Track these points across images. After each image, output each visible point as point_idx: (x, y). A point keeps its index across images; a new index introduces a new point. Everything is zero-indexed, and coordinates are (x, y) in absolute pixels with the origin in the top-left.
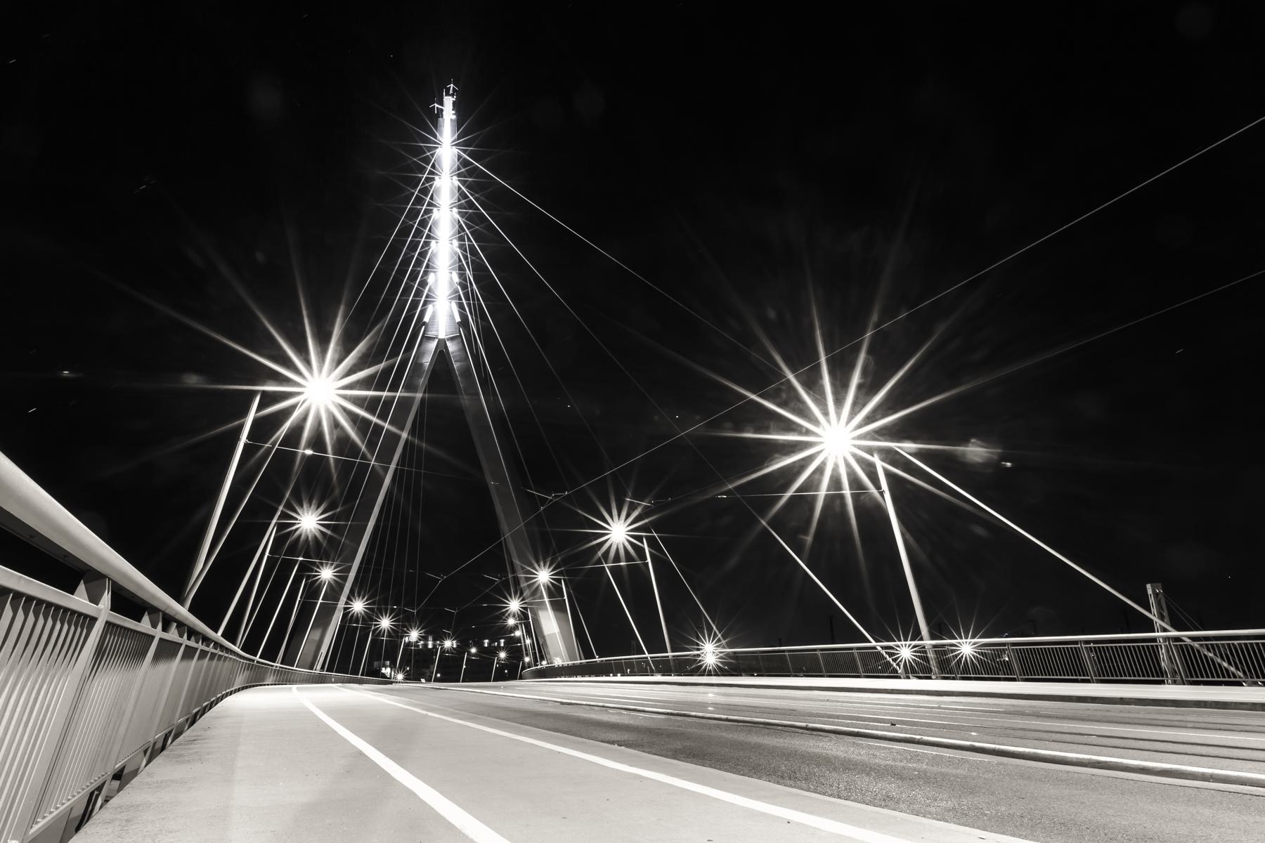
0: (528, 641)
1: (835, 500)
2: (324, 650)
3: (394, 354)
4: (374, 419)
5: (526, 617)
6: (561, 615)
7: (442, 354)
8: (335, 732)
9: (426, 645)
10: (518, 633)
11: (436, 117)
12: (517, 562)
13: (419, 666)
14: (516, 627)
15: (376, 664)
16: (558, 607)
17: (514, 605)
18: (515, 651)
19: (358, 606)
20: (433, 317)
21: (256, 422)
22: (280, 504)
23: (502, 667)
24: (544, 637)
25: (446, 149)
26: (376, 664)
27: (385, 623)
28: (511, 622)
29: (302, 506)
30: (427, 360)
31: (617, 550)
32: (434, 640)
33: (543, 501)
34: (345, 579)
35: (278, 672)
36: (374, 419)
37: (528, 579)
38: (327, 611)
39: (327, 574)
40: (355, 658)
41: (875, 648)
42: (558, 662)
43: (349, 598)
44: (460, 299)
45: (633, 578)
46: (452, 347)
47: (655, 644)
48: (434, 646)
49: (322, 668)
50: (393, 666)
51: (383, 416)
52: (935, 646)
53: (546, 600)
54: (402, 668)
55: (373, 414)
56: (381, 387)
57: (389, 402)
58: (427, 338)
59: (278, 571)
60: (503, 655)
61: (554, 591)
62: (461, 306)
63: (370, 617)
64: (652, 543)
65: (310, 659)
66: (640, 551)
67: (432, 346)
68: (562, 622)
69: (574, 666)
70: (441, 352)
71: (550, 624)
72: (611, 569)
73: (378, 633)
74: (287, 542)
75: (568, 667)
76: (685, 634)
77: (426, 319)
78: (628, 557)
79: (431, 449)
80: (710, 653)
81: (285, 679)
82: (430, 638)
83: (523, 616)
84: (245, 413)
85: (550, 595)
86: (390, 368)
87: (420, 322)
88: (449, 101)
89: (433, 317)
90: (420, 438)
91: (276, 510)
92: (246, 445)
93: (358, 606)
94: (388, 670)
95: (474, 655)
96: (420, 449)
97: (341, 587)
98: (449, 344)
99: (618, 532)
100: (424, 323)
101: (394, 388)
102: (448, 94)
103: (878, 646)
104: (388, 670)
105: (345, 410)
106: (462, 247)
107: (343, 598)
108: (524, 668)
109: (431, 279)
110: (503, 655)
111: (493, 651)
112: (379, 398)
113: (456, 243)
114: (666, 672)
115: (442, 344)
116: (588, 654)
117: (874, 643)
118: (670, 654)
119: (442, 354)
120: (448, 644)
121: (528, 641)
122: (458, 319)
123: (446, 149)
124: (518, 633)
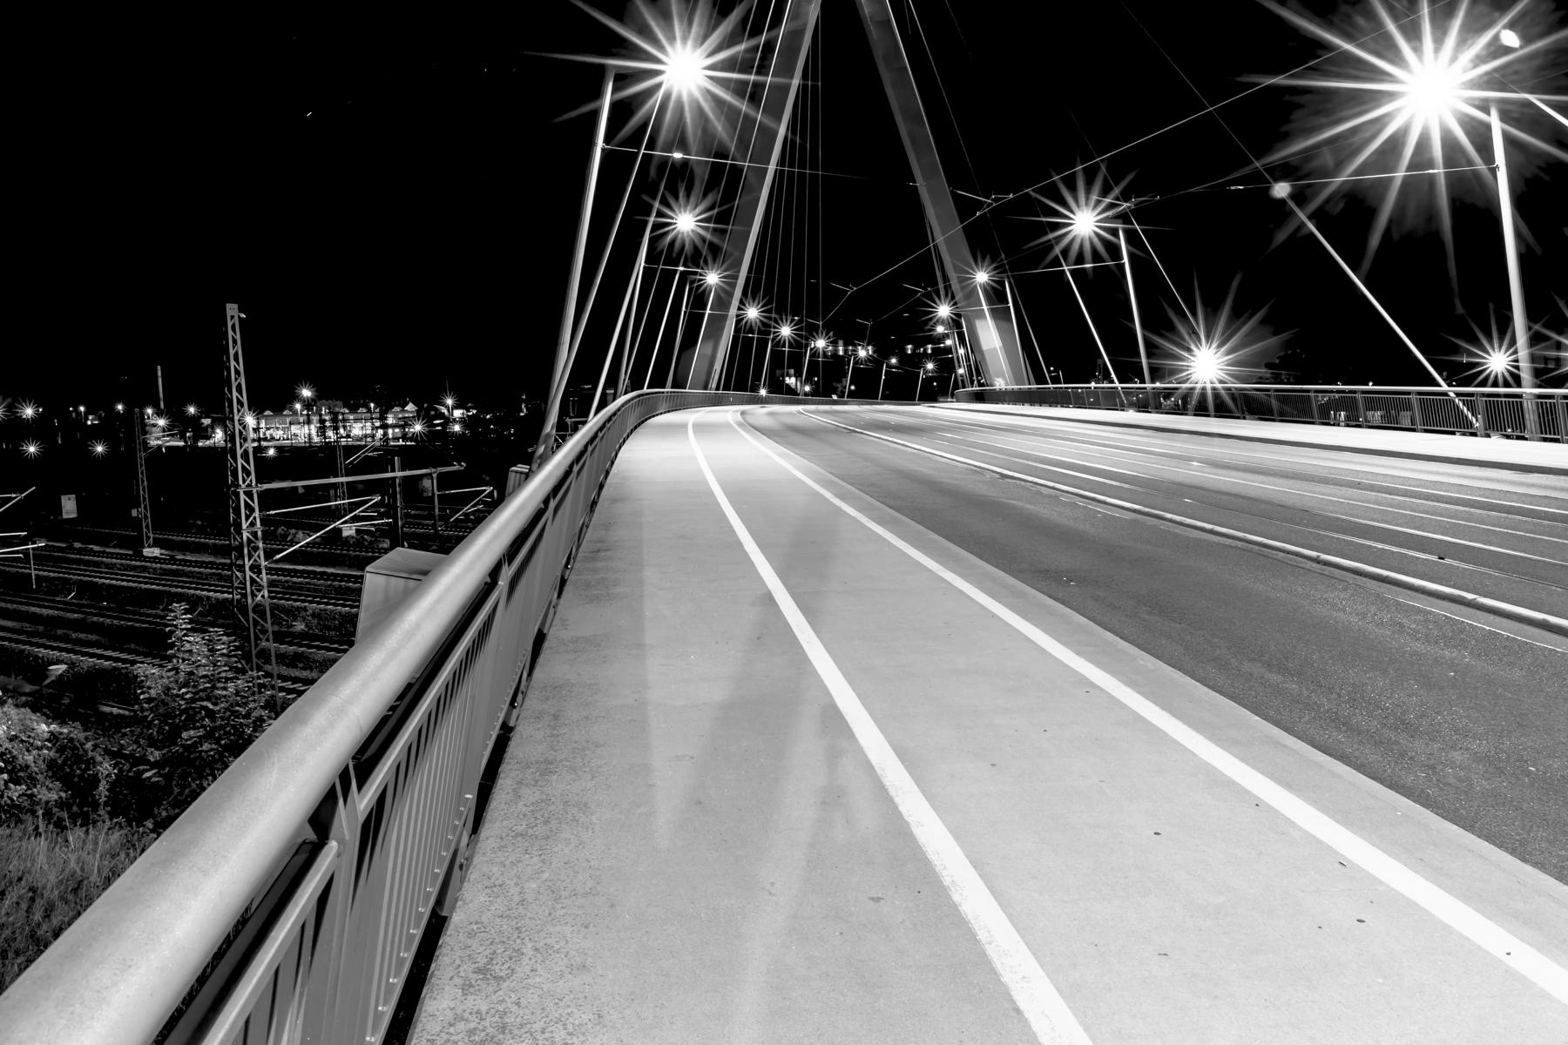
0: (961, 351)
2: (717, 367)
3: (776, 22)
5: (959, 326)
6: (1004, 324)
8: (739, 544)
10: (949, 342)
13: (828, 381)
14: (946, 336)
15: (778, 372)
16: (1000, 315)
17: (944, 310)
18: (946, 362)
21: (613, 105)
22: (649, 215)
23: (928, 381)
24: (981, 352)
26: (778, 372)
27: (786, 331)
31: (1081, 246)
32: (846, 345)
33: (980, 205)
34: (733, 286)
35: (671, 397)
38: (718, 322)
39: (712, 278)
40: (753, 371)
41: (1445, 394)
42: (1000, 384)
43: (741, 302)
45: (1102, 283)
47: (1129, 371)
48: (846, 351)
50: (798, 375)
52: (1540, 396)
53: (985, 307)
54: (808, 380)
59: (657, 284)
61: (995, 294)
63: (765, 328)
64: (1132, 237)
65: (703, 378)
66: (1114, 250)
68: (1004, 334)
69: (1020, 392)
71: (990, 336)
72: (1073, 272)
73: (778, 343)
74: (667, 254)
75: (1013, 392)
78: (1096, 257)
80: (1207, 364)
81: (679, 405)
82: (841, 342)
83: (955, 322)
84: (598, 94)
85: (990, 301)
91: (646, 223)
92: (603, 150)
93: (753, 313)
94: (793, 380)
97: (731, 295)
99: (1084, 222)
103: (1451, 391)
104: (793, 380)
105: (711, 78)
107: (733, 311)
108: (956, 387)
110: (930, 366)
111: (918, 360)
114: (1143, 407)
116: (1040, 379)
117: (1445, 387)
118: (1148, 385)
120: (862, 353)
121: (961, 351)
124: (949, 342)
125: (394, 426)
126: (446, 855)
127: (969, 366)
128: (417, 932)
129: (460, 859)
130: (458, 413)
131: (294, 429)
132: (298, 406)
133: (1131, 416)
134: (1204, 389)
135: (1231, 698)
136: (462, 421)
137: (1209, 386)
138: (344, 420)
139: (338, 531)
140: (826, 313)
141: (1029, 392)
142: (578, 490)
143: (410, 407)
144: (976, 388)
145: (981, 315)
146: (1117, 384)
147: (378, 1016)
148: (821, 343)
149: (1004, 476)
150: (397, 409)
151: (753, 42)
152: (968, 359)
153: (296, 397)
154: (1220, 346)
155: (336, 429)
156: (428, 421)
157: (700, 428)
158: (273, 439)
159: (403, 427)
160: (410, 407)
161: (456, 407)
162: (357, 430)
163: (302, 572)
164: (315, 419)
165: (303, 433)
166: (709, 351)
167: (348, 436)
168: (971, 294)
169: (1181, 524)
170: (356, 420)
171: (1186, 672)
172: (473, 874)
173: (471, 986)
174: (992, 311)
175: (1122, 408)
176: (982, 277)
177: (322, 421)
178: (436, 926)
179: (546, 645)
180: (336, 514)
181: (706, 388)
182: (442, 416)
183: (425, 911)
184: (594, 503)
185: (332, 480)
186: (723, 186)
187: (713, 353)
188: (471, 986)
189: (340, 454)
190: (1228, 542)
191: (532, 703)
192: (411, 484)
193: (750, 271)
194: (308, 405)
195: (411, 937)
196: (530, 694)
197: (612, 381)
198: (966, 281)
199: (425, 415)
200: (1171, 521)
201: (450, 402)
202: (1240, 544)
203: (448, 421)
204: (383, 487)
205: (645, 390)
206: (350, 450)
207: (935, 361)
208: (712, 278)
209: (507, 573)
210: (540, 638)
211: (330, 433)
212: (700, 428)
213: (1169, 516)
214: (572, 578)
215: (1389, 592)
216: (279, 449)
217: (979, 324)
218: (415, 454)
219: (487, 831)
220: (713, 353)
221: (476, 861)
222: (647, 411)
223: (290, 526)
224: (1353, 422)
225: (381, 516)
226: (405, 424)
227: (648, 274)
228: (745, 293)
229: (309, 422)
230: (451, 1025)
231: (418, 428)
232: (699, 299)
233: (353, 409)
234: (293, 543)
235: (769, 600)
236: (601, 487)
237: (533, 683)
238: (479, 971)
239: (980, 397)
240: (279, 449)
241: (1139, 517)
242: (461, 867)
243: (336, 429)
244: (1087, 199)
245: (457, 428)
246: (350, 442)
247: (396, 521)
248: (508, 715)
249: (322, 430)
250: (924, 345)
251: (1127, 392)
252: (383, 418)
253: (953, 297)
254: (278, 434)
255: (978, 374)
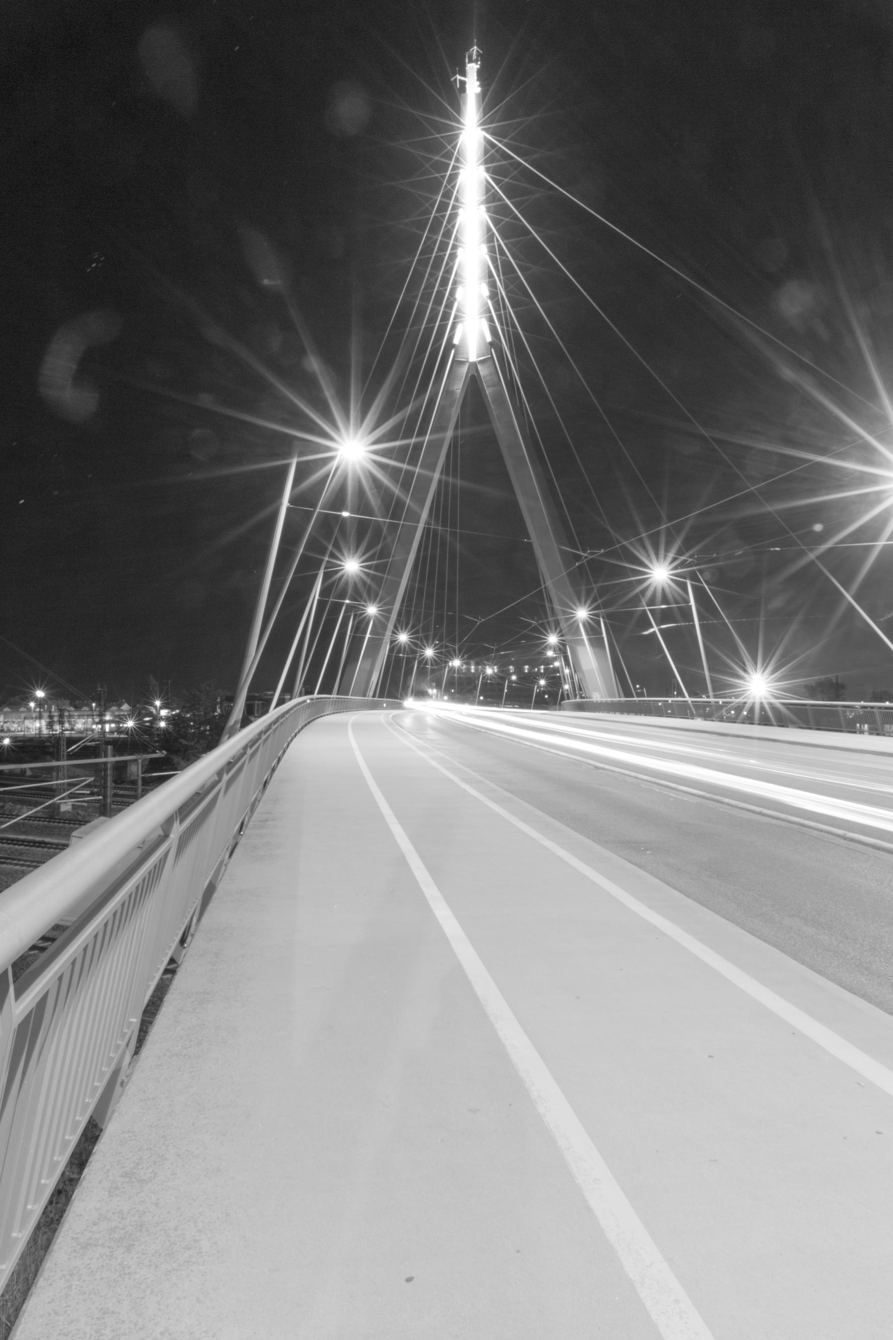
0: (567, 671)
1: (839, 479)
4: (405, 466)
7: (474, 382)
8: (381, 817)
9: (468, 669)
10: (557, 664)
11: (455, 95)
12: (557, 607)
14: (554, 659)
16: (596, 642)
17: (553, 639)
18: (555, 680)
19: (403, 638)
20: (463, 340)
23: (540, 695)
25: (472, 134)
27: (429, 652)
28: (550, 654)
29: (343, 555)
30: (459, 387)
34: (388, 619)
35: (336, 702)
36: (405, 466)
37: (567, 620)
38: (375, 645)
39: (372, 610)
42: (597, 697)
44: (490, 312)
45: (673, 612)
46: (483, 371)
47: (696, 686)
48: (476, 670)
49: (374, 696)
51: (413, 461)
53: (585, 637)
55: (403, 462)
56: (408, 434)
57: (417, 447)
58: (457, 363)
59: (328, 613)
60: (542, 682)
61: (592, 629)
62: (491, 320)
67: (464, 369)
68: (600, 657)
70: (473, 377)
74: (334, 588)
76: (726, 667)
77: (456, 341)
79: (466, 484)
80: (759, 685)
81: (342, 707)
83: (561, 649)
86: (416, 413)
87: (450, 345)
88: (472, 68)
89: (463, 340)
90: (455, 476)
95: (515, 682)
96: (454, 486)
98: (479, 367)
99: (660, 574)
100: (454, 346)
101: (422, 432)
102: (471, 61)
106: (492, 250)
107: (388, 633)
108: (563, 699)
109: (459, 294)
112: (408, 446)
113: (484, 249)
114: (707, 717)
115: (474, 366)
116: (627, 693)
119: (474, 382)
120: (489, 671)
122: (489, 339)
123: (472, 134)
124: (557, 664)
125: (110, 722)
126: (108, 1071)
127: (573, 683)
128: (73, 1139)
129: (122, 1077)
130: (164, 713)
131: (28, 723)
132: (32, 705)
133: (698, 723)
134: (754, 703)
135: (775, 946)
136: (167, 719)
137: (764, 701)
138: (70, 716)
139: (55, 807)
140: (460, 640)
141: (620, 703)
142: (250, 773)
143: (126, 707)
144: (578, 700)
145: (581, 642)
146: (688, 699)
147: (26, 1214)
148: (456, 663)
149: (597, 768)
150: (114, 708)
151: (420, 439)
152: (572, 678)
153: (29, 697)
154: (773, 672)
155: (61, 723)
156: (139, 716)
157: (357, 726)
158: (9, 731)
159: (118, 723)
160: (126, 707)
161: (163, 707)
162: (80, 725)
163: (23, 841)
164: (46, 715)
165: (36, 727)
166: (367, 666)
167: (72, 729)
168: (574, 628)
169: (736, 807)
170: (80, 716)
171: (738, 924)
172: (131, 1089)
173: (117, 1188)
174: (590, 640)
175: (692, 717)
176: (582, 614)
177: (51, 717)
178: (91, 1134)
179: (215, 895)
180: (50, 792)
181: (364, 695)
182: (150, 714)
183: (83, 1121)
184: (266, 784)
185: (54, 763)
186: (367, 537)
187: (371, 670)
188: (117, 1188)
189: (63, 743)
190: (774, 821)
191: (196, 943)
192: (120, 768)
193: (402, 605)
194: (40, 703)
195: (66, 1143)
196: (197, 936)
197: (289, 689)
198: (570, 618)
199: (138, 715)
200: (728, 804)
201: (158, 703)
202: (783, 823)
203: (156, 718)
204: (97, 769)
205: (315, 695)
206: (71, 741)
207: (547, 679)
208: (372, 610)
209: (178, 829)
210: (210, 890)
211: (57, 727)
212: (358, 727)
213: (726, 800)
214: (243, 841)
215: (853, 845)
216: (14, 739)
217: (580, 650)
218: (123, 745)
219: (145, 1051)
220: (371, 670)
221: (134, 1077)
222: (317, 711)
223: (15, 802)
224: (876, 731)
225: (92, 794)
226: (119, 719)
227: (321, 605)
228: (398, 620)
229: (40, 717)
230: (95, 1224)
231: (130, 724)
232: (361, 627)
233: (77, 708)
234: (12, 816)
235: (402, 861)
236: (273, 770)
237: (201, 927)
238: (126, 1175)
239: (581, 707)
240: (14, 739)
241: (704, 801)
242: (122, 1084)
243: (61, 723)
244: (665, 556)
245: (163, 724)
246: (74, 734)
247: (105, 797)
248: (177, 951)
249: (50, 725)
250: (538, 665)
251: (697, 706)
252: (101, 715)
253: (561, 631)
254: (14, 727)
255: (580, 689)
